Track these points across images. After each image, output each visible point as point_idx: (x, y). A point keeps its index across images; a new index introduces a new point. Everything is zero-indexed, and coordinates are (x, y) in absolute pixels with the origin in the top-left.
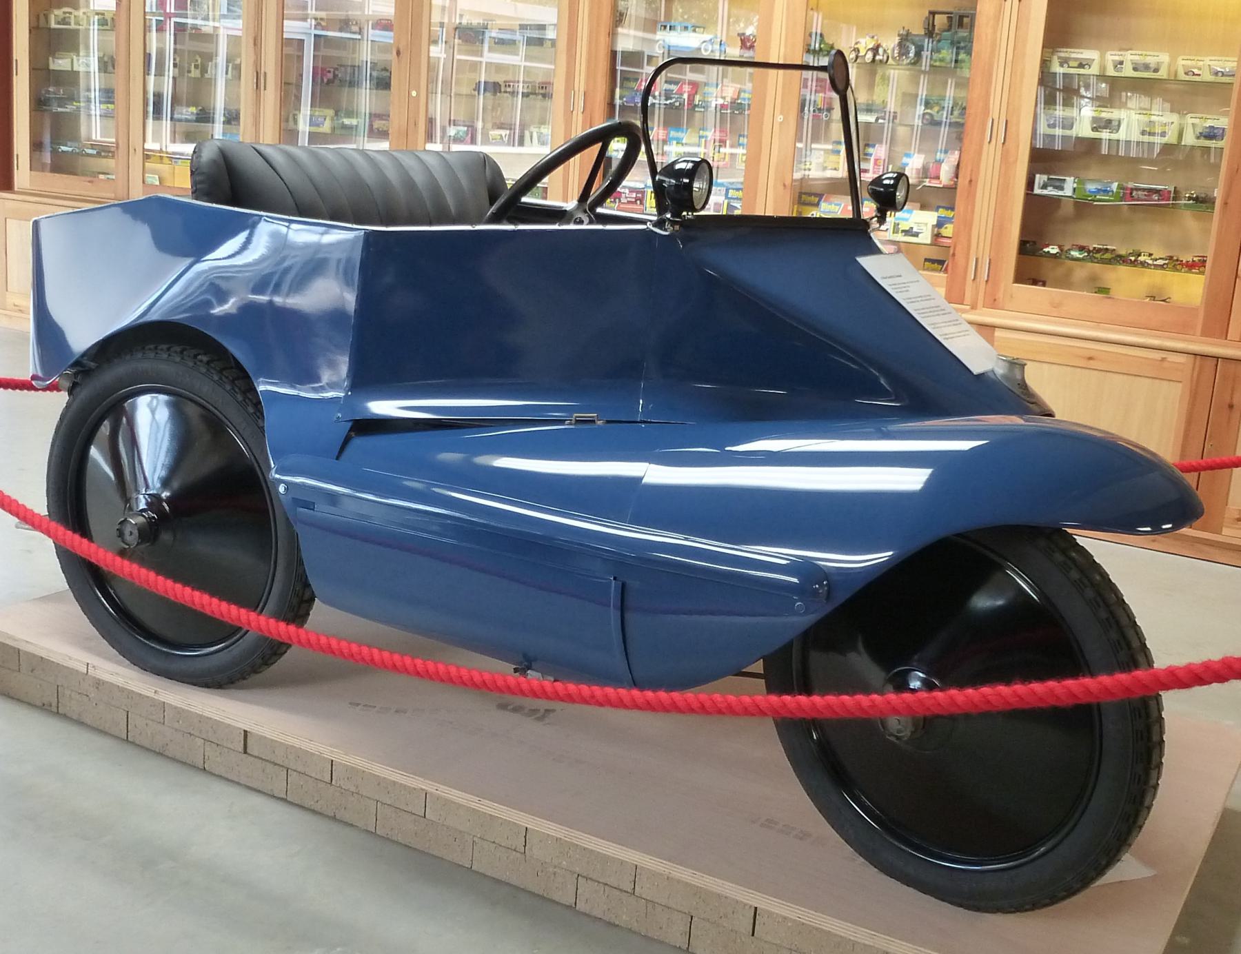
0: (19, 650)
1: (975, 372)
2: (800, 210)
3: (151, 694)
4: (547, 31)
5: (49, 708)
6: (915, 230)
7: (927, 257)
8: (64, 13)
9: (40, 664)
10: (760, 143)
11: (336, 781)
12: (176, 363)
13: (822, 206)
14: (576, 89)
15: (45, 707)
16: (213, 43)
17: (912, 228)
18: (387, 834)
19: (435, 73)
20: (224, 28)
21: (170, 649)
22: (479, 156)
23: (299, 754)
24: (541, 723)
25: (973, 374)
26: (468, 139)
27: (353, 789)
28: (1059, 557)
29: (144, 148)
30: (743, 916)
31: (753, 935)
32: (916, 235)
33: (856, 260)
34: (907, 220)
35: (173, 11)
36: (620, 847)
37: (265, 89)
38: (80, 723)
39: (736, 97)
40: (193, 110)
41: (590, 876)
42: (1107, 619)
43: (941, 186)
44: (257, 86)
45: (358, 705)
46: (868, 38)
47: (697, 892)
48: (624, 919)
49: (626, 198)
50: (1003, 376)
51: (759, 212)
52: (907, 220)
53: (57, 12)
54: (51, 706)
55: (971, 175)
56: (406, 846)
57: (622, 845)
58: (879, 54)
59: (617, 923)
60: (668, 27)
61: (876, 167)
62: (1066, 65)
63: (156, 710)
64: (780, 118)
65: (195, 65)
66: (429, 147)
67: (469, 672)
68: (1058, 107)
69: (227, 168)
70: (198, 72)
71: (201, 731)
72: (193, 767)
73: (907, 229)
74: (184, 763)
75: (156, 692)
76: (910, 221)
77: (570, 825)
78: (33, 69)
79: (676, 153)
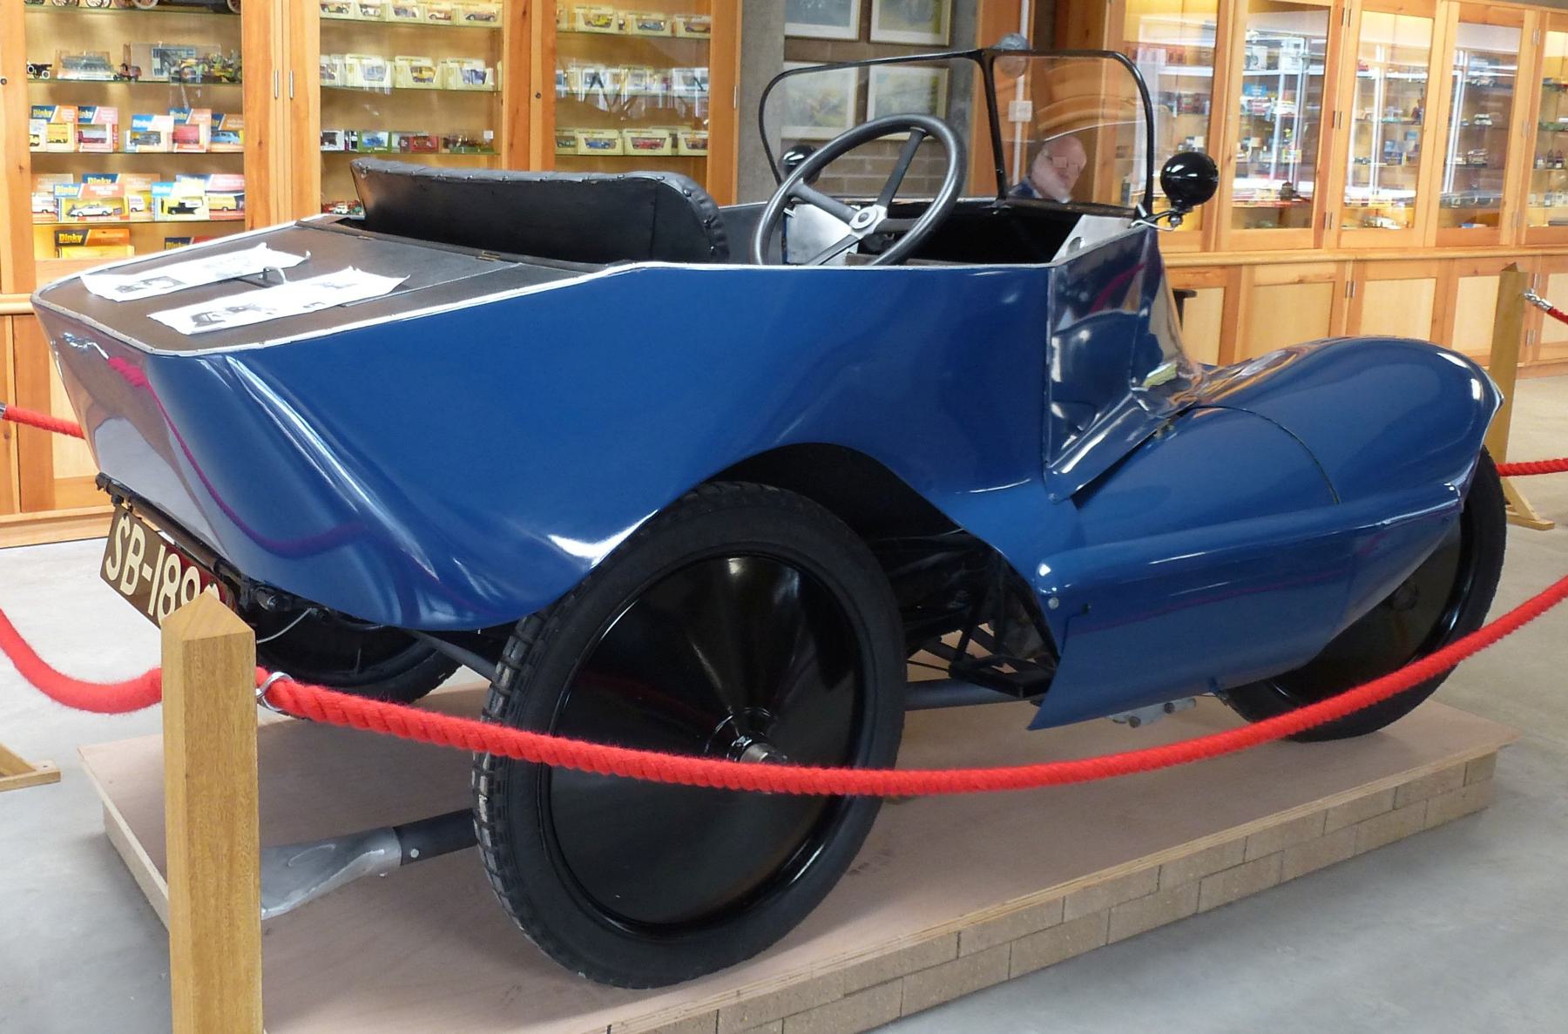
6: (187, 206)
7: (168, 237)
18: (840, 1009)
29: (1429, 74)
32: (191, 211)
34: (168, 195)
43: (205, 151)
55: (260, 136)
62: (326, 9)
63: (241, 882)
66: (109, 141)
67: (859, 788)
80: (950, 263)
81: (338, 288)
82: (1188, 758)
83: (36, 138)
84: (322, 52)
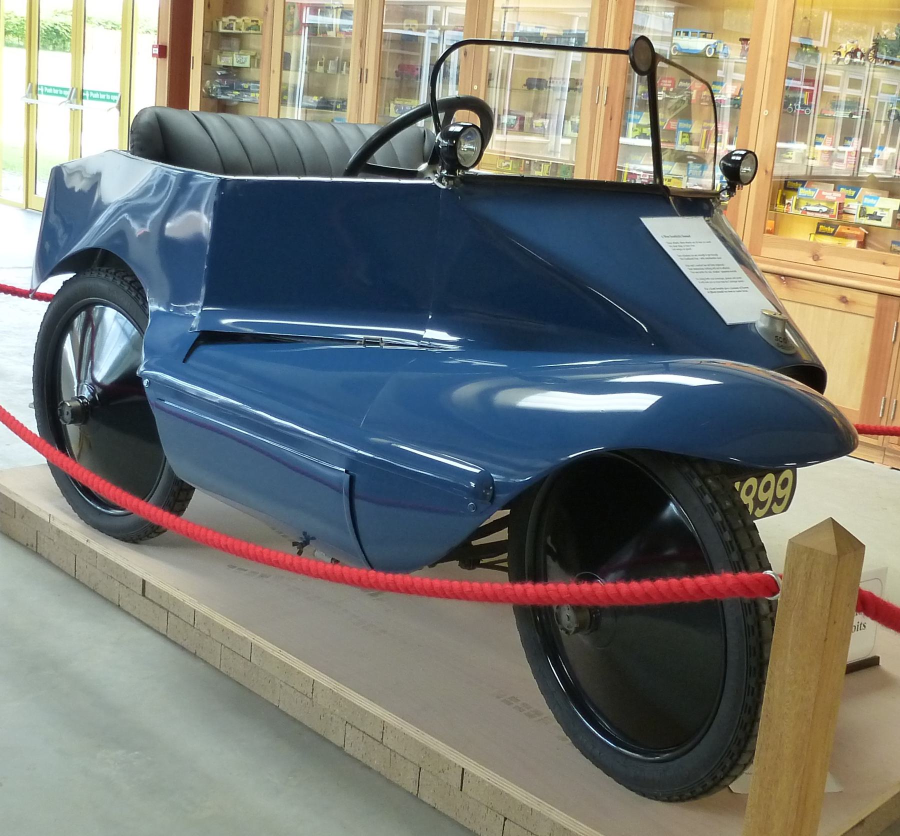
0: (15, 502)
1: (728, 322)
2: (784, 194)
3: (85, 542)
4: (319, 23)
5: (31, 548)
6: (878, 214)
8: (230, 20)
9: (25, 514)
10: (749, 130)
11: (197, 624)
12: (108, 281)
13: (800, 192)
14: (601, 85)
15: (28, 547)
16: (419, 52)
17: (876, 213)
19: (420, 64)
20: (429, 37)
21: (96, 504)
22: (420, 131)
23: (175, 601)
24: (374, 598)
25: (725, 324)
26: (517, 127)
27: (207, 633)
28: (697, 483)
30: (455, 772)
31: (461, 790)
33: (640, 220)
34: (873, 205)
35: (446, 24)
36: (369, 701)
37: (366, 82)
38: (49, 562)
39: (737, 94)
40: (316, 99)
41: (354, 724)
42: (730, 542)
44: (361, 80)
45: (234, 567)
46: (848, 43)
47: (425, 749)
48: (375, 764)
49: (641, 179)
50: (763, 329)
51: (591, 179)
52: (873, 205)
53: (224, 19)
54: (32, 546)
56: (237, 682)
57: (371, 700)
58: (857, 57)
59: (371, 766)
60: (690, 33)
61: (850, 157)
64: (765, 112)
65: (320, 63)
68: (845, 100)
69: (161, 131)
70: (322, 68)
71: (117, 576)
72: (112, 603)
73: (872, 213)
74: (106, 599)
75: (87, 541)
76: (876, 206)
77: (339, 679)
78: (205, 64)
79: (26, 97)
80: (357, 157)
81: (110, 109)
82: (285, 464)
83: (888, 163)
84: (848, 88)
